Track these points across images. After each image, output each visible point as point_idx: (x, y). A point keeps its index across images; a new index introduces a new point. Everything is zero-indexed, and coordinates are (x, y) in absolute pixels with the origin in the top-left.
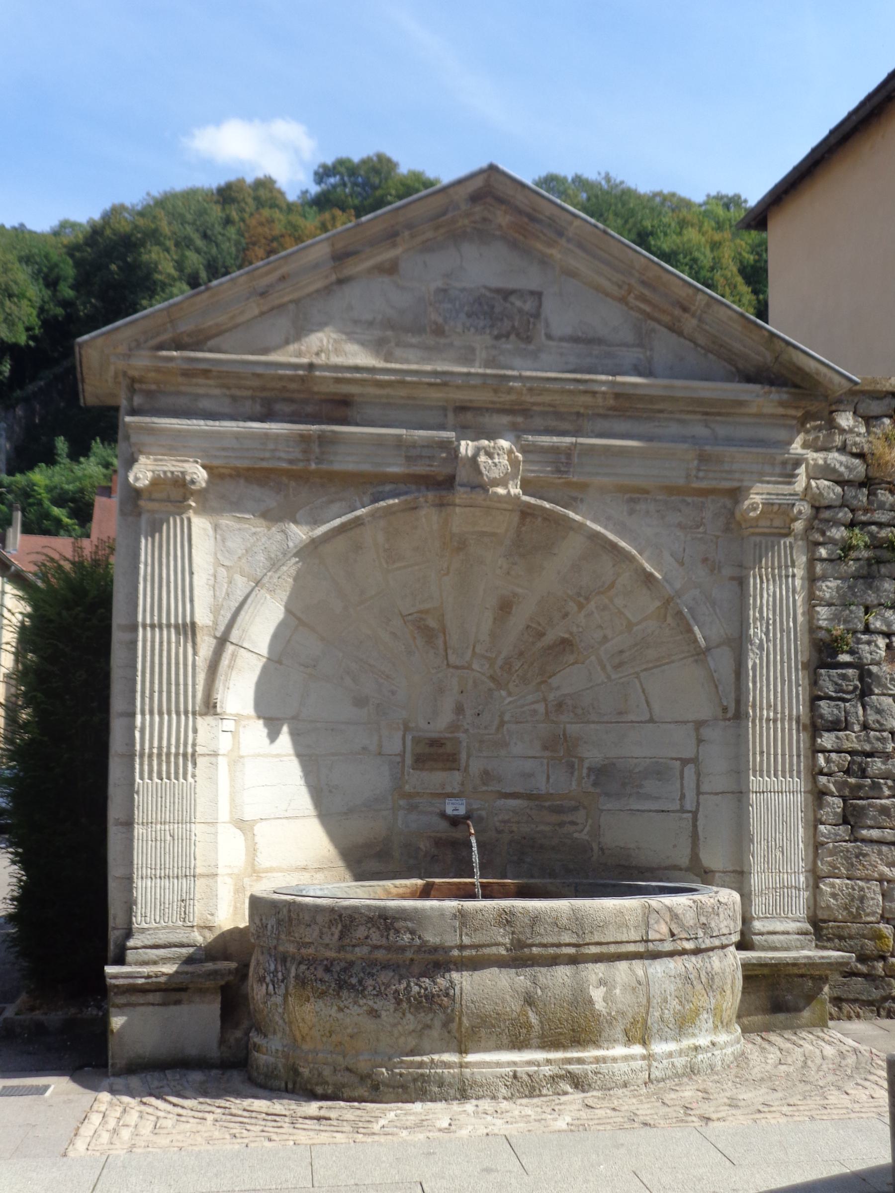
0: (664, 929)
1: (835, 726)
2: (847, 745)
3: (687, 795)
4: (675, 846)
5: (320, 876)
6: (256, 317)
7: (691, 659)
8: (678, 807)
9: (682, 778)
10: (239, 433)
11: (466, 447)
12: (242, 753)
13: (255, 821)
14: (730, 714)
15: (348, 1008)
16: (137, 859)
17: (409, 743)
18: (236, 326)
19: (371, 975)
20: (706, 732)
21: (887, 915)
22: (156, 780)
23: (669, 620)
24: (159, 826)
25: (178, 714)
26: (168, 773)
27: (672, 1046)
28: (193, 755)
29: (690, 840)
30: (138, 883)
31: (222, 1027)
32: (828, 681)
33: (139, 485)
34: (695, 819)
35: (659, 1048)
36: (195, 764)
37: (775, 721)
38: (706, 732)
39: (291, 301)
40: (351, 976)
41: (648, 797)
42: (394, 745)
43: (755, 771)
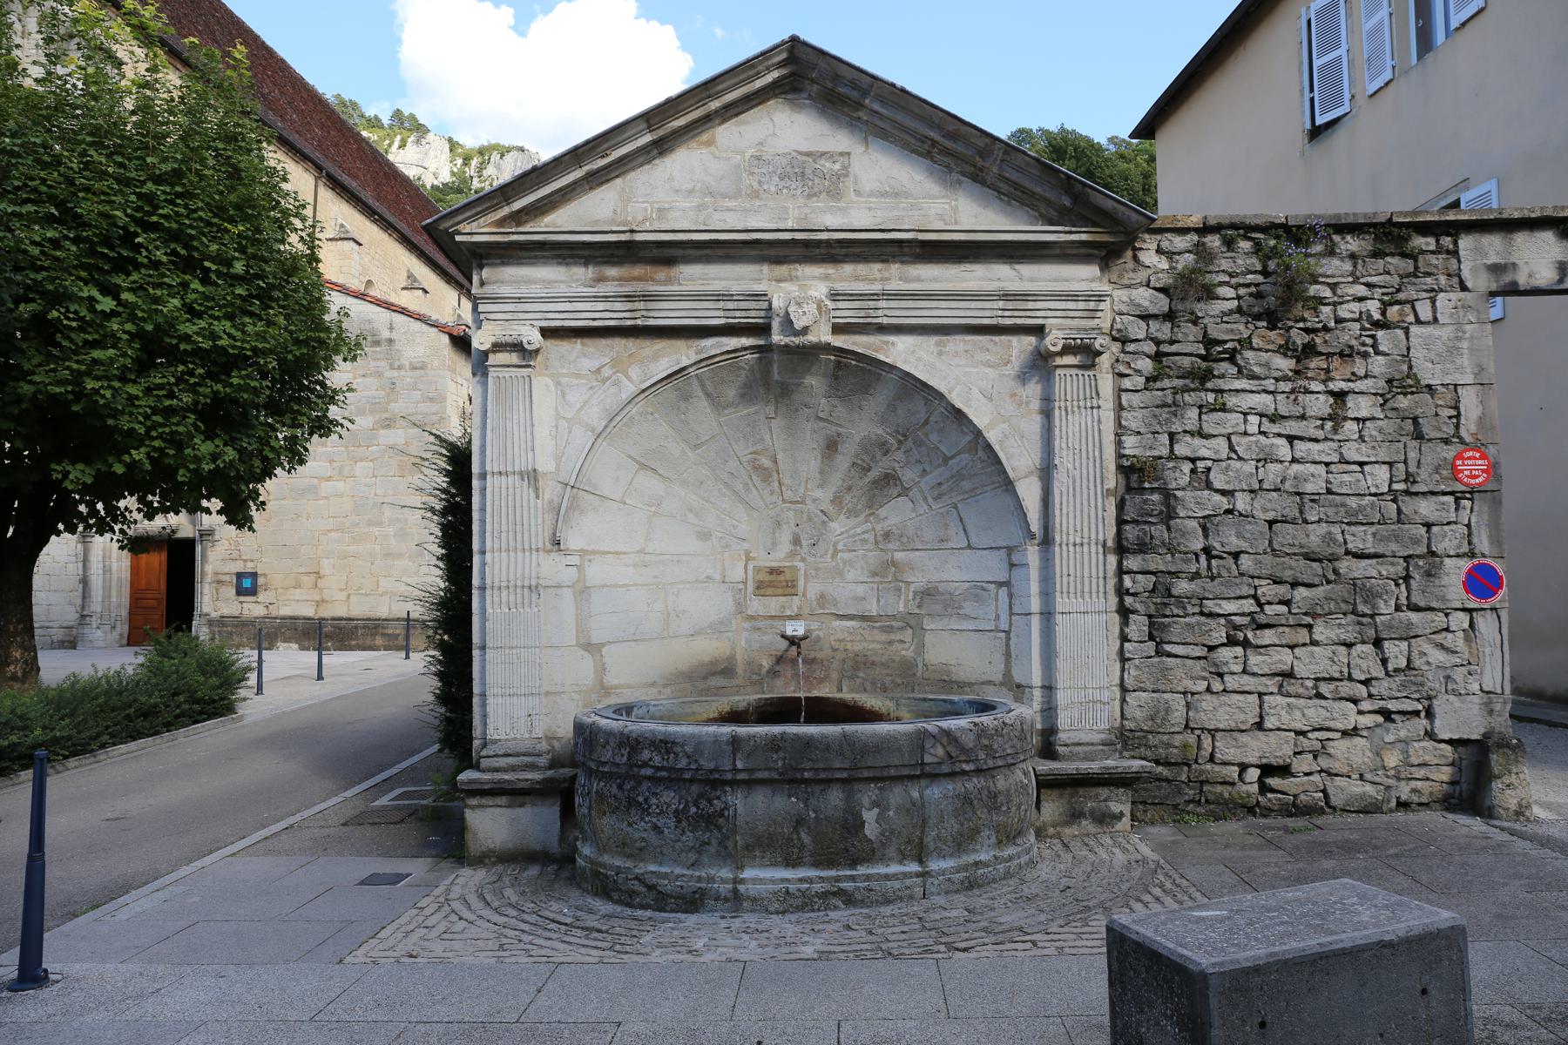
0: (940, 751)
1: (1143, 548)
2: (1152, 567)
5: (668, 691)
13: (603, 645)
17: (750, 573)
21: (1192, 725)
23: (980, 453)
27: (950, 863)
31: (562, 826)
32: (1133, 503)
34: (1008, 639)
35: (935, 865)
42: (737, 573)
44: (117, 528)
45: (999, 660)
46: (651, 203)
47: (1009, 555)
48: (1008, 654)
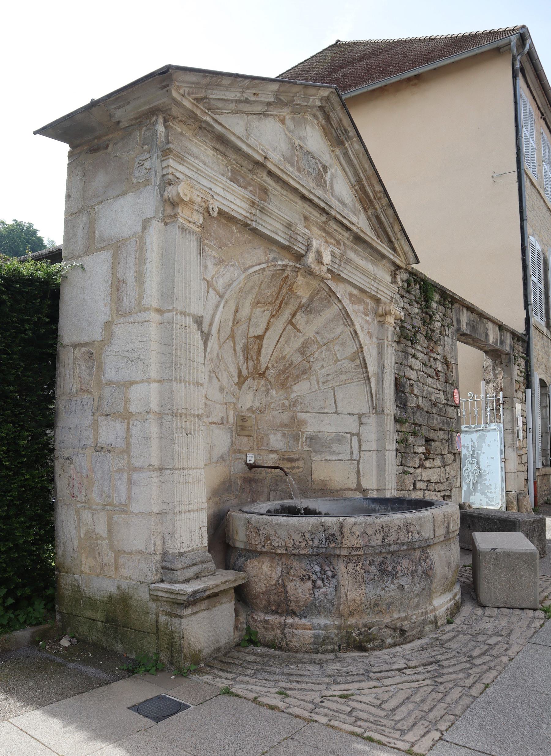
8: (350, 458)
9: (351, 443)
15: (388, 587)
19: (399, 563)
20: (364, 420)
34: (358, 464)
38: (364, 420)
40: (388, 566)
41: (334, 453)
44: (112, 157)
45: (354, 475)
47: (359, 418)
48: (358, 472)
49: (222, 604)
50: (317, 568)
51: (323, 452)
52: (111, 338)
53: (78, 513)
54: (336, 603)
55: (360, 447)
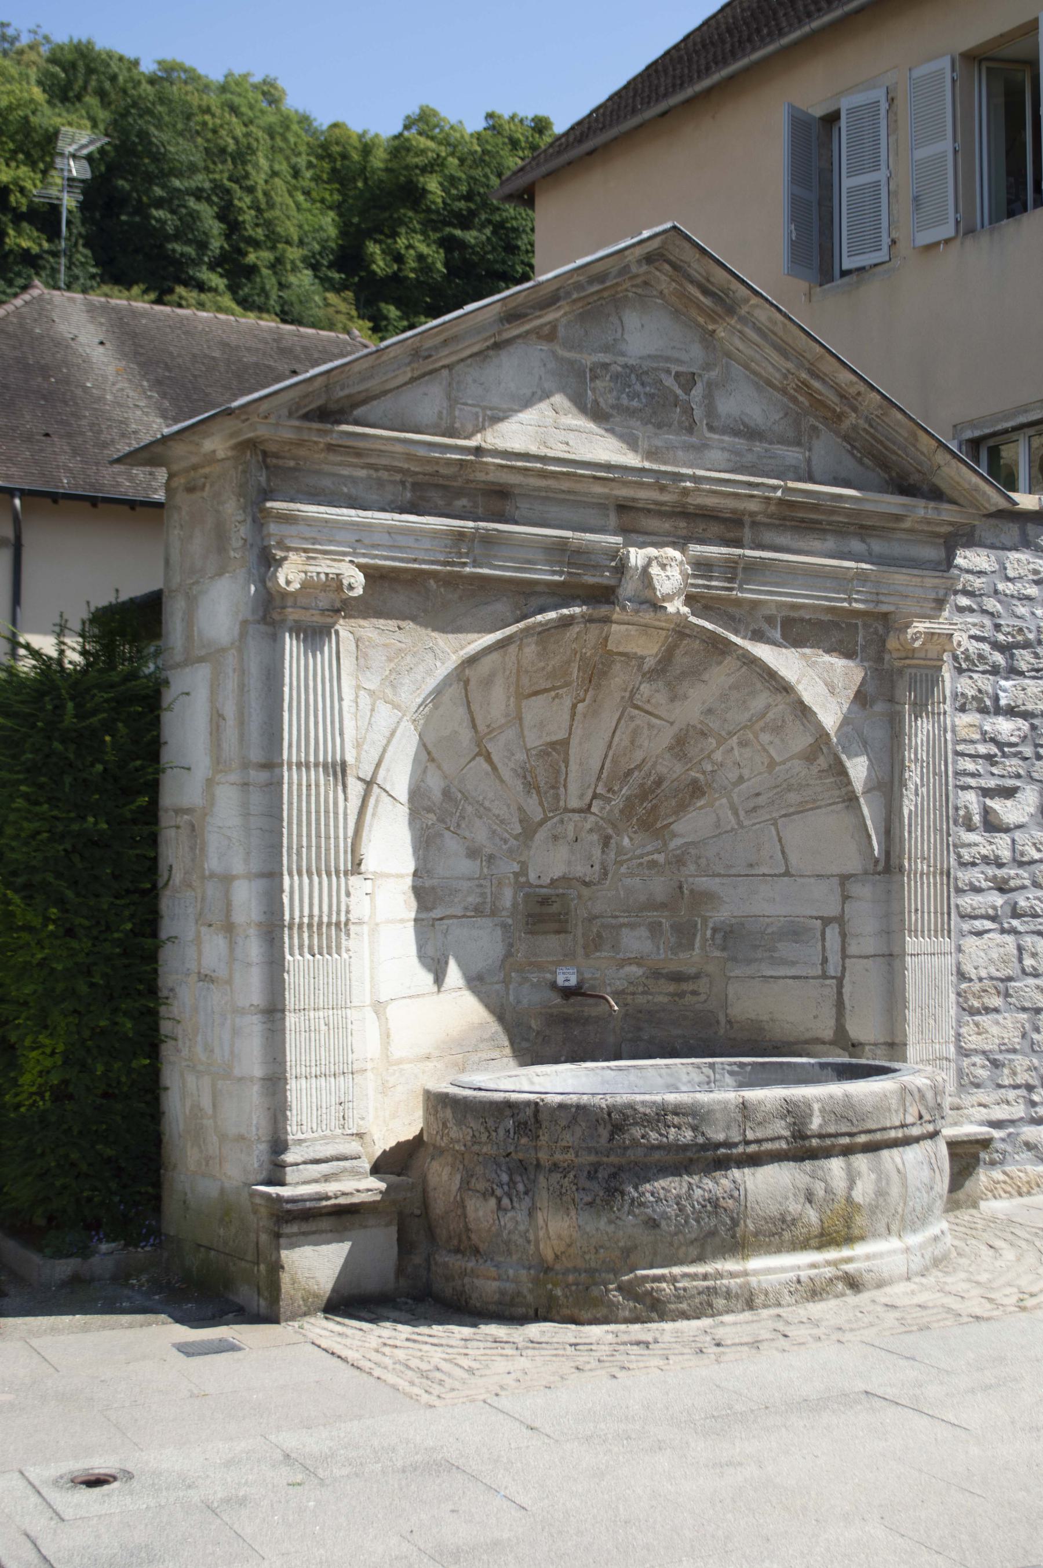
3: (830, 959)
4: (815, 1017)
6: (405, 384)
7: (840, 806)
8: (820, 972)
9: (823, 939)
10: (391, 527)
11: (637, 556)
12: (378, 921)
14: (880, 868)
16: (290, 1056)
18: (385, 393)
22: (308, 956)
24: (312, 1013)
25: (329, 874)
26: (320, 947)
28: (346, 924)
29: (834, 1010)
30: (292, 1085)
33: (291, 588)
36: (348, 935)
37: (928, 874)
39: (444, 367)
41: (784, 962)
43: (910, 931)
46: (484, 408)
47: (842, 884)
49: (366, 1227)
50: (505, 1178)
51: (756, 960)
52: (212, 805)
53: (182, 1075)
54: (532, 1237)
55: (843, 949)
